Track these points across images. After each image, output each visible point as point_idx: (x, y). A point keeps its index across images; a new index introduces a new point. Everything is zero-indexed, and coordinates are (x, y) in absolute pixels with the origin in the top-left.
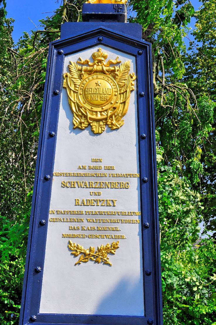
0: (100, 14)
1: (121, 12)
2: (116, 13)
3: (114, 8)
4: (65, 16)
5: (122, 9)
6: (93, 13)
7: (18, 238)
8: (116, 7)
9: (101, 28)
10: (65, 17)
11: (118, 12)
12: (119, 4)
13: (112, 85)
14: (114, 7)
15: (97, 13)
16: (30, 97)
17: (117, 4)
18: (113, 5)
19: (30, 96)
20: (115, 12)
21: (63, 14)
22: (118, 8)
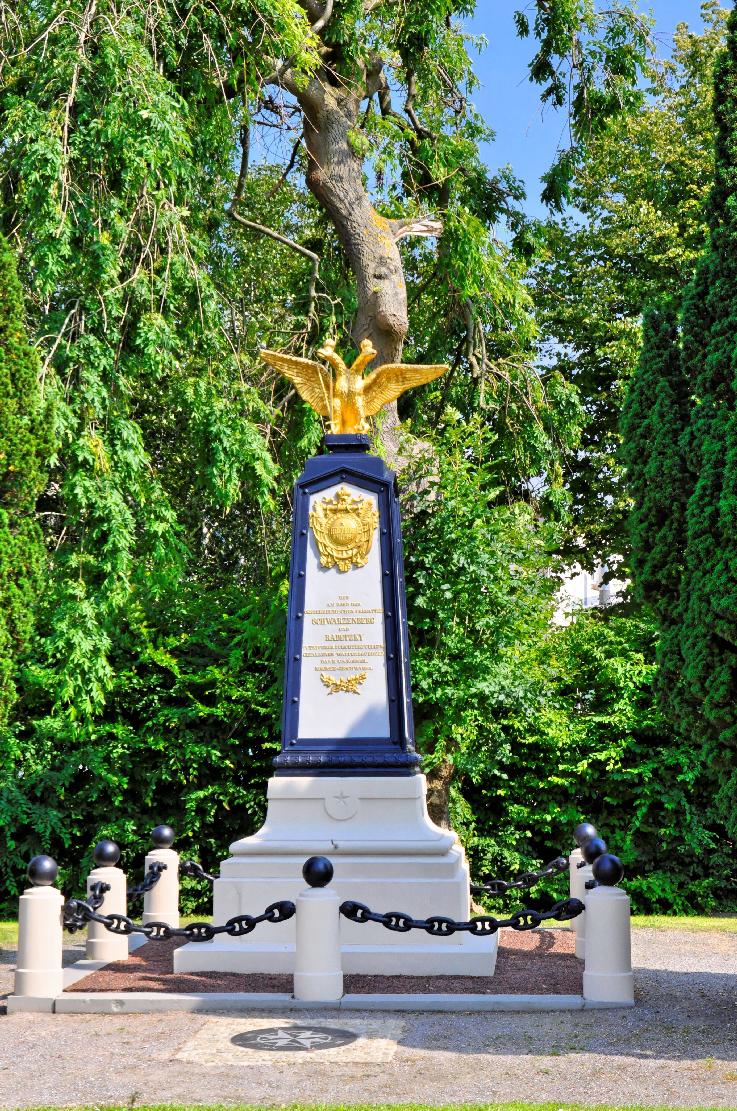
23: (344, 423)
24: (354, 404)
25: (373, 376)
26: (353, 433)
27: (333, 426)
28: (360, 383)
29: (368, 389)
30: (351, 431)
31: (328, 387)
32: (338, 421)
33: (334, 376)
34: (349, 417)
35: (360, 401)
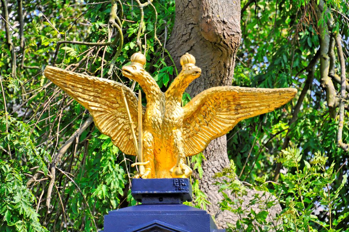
0: (155, 194)
1: (183, 190)
2: (178, 192)
3: (174, 185)
4: (114, 20)
5: (185, 185)
6: (146, 192)
7: (29, 49)
8: (176, 182)
9: (156, 224)
10: (116, 21)
11: (179, 190)
12: (181, 179)
13: (160, 202)
14: (174, 183)
15: (151, 192)
16: (50, 179)
17: (178, 179)
18: (173, 180)
19: (51, 176)
20: (176, 190)
21: (111, 16)
22: (180, 185)
23: (156, 165)
24: (170, 139)
25: (196, 101)
26: (169, 177)
27: (142, 168)
28: (179, 112)
29: (188, 120)
30: (164, 175)
31: (135, 116)
32: (149, 161)
33: (144, 102)
34: (164, 158)
35: (179, 135)
